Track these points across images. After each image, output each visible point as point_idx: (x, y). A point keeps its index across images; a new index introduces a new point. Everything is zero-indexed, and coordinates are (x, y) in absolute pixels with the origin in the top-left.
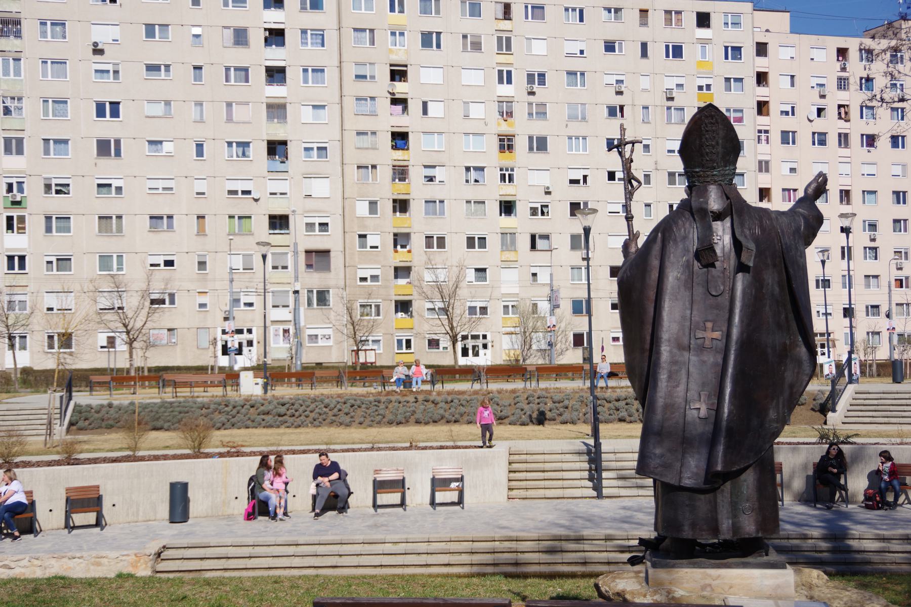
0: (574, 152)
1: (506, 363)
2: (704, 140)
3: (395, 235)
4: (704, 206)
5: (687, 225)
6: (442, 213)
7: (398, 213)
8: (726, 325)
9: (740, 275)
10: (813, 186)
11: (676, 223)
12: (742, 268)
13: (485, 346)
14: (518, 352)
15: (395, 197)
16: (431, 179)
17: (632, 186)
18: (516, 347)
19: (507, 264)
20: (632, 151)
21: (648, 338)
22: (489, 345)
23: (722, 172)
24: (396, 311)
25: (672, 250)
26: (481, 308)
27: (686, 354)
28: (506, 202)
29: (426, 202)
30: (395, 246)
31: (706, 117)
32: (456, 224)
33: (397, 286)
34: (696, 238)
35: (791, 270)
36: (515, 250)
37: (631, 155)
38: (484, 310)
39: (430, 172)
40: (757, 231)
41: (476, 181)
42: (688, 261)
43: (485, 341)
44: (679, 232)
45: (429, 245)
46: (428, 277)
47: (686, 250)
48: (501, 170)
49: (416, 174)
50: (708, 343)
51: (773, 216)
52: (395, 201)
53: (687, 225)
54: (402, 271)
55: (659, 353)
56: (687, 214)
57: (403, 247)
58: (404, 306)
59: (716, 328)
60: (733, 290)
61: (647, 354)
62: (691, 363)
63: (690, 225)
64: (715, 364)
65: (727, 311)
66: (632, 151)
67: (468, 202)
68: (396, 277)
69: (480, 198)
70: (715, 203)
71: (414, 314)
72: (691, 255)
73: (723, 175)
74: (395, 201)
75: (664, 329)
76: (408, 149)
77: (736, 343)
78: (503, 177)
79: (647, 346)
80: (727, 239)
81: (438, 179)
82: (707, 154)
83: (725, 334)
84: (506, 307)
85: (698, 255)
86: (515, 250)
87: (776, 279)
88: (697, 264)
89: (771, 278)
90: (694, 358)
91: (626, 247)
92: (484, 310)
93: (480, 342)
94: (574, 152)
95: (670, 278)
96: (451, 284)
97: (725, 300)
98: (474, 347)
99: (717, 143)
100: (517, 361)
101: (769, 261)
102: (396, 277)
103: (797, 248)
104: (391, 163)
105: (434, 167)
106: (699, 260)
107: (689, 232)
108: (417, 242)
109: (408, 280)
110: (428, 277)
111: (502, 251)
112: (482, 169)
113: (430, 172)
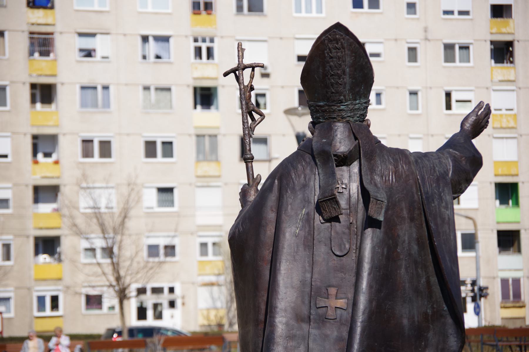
0: (303, 14)
1: (204, 330)
2: (328, 68)
3: (35, 137)
4: (327, 148)
5: (308, 171)
6: (107, 104)
7: (38, 105)
8: (352, 290)
9: (369, 231)
10: (473, 118)
11: (295, 168)
12: (371, 222)
13: (172, 304)
14: (222, 312)
15: (35, 80)
16: (89, 53)
17: (253, 119)
18: (219, 304)
19: (205, 181)
20: (252, 77)
21: (263, 307)
22: (179, 303)
23: (351, 107)
24: (37, 253)
25: (290, 201)
26: (166, 247)
27: (305, 326)
28: (203, 89)
29: (83, 88)
30: (35, 154)
31: (330, 41)
32: (127, 123)
33: (38, 216)
34: (317, 186)
35: (432, 225)
36: (217, 160)
37: (251, 82)
38: (170, 250)
40: (392, 178)
41: (158, 57)
42: (308, 214)
43: (172, 297)
44: (298, 180)
45: (87, 153)
46: (84, 203)
47: (306, 201)
48: (196, 40)
49: (66, 46)
50: (331, 313)
51: (412, 159)
52: (33, 86)
53: (308, 171)
54: (44, 193)
55: (273, 325)
56: (308, 157)
57: (47, 155)
58: (48, 245)
59: (340, 295)
60: (360, 249)
61: (262, 326)
62: (311, 338)
63: (311, 171)
64: (339, 339)
65: (353, 274)
66: (252, 77)
67: (147, 88)
68: (36, 200)
69: (163, 83)
70: (342, 143)
71: (63, 257)
72: (312, 206)
73: (352, 110)
74: (33, 86)
75: (280, 297)
76: (52, 8)
77: (363, 314)
78: (198, 52)
79: (262, 317)
80: (355, 187)
81: (99, 54)
82: (332, 85)
83: (351, 302)
84: (204, 245)
85: (319, 208)
86: (217, 160)
87: (414, 235)
88: (318, 218)
89: (406, 232)
90: (313, 331)
91: (244, 194)
92: (170, 250)
93: (164, 298)
94: (303, 14)
95: (288, 235)
96: (116, 211)
97: (350, 261)
98: (156, 306)
99: (344, 72)
100: (220, 326)
101: (405, 213)
102: (36, 200)
103: (441, 198)
104: (26, 28)
105: (93, 35)
106: (320, 214)
107: (310, 179)
108: (69, 149)
109: (54, 206)
110: (84, 203)
111: (198, 161)
112: (165, 39)
113: (87, 43)
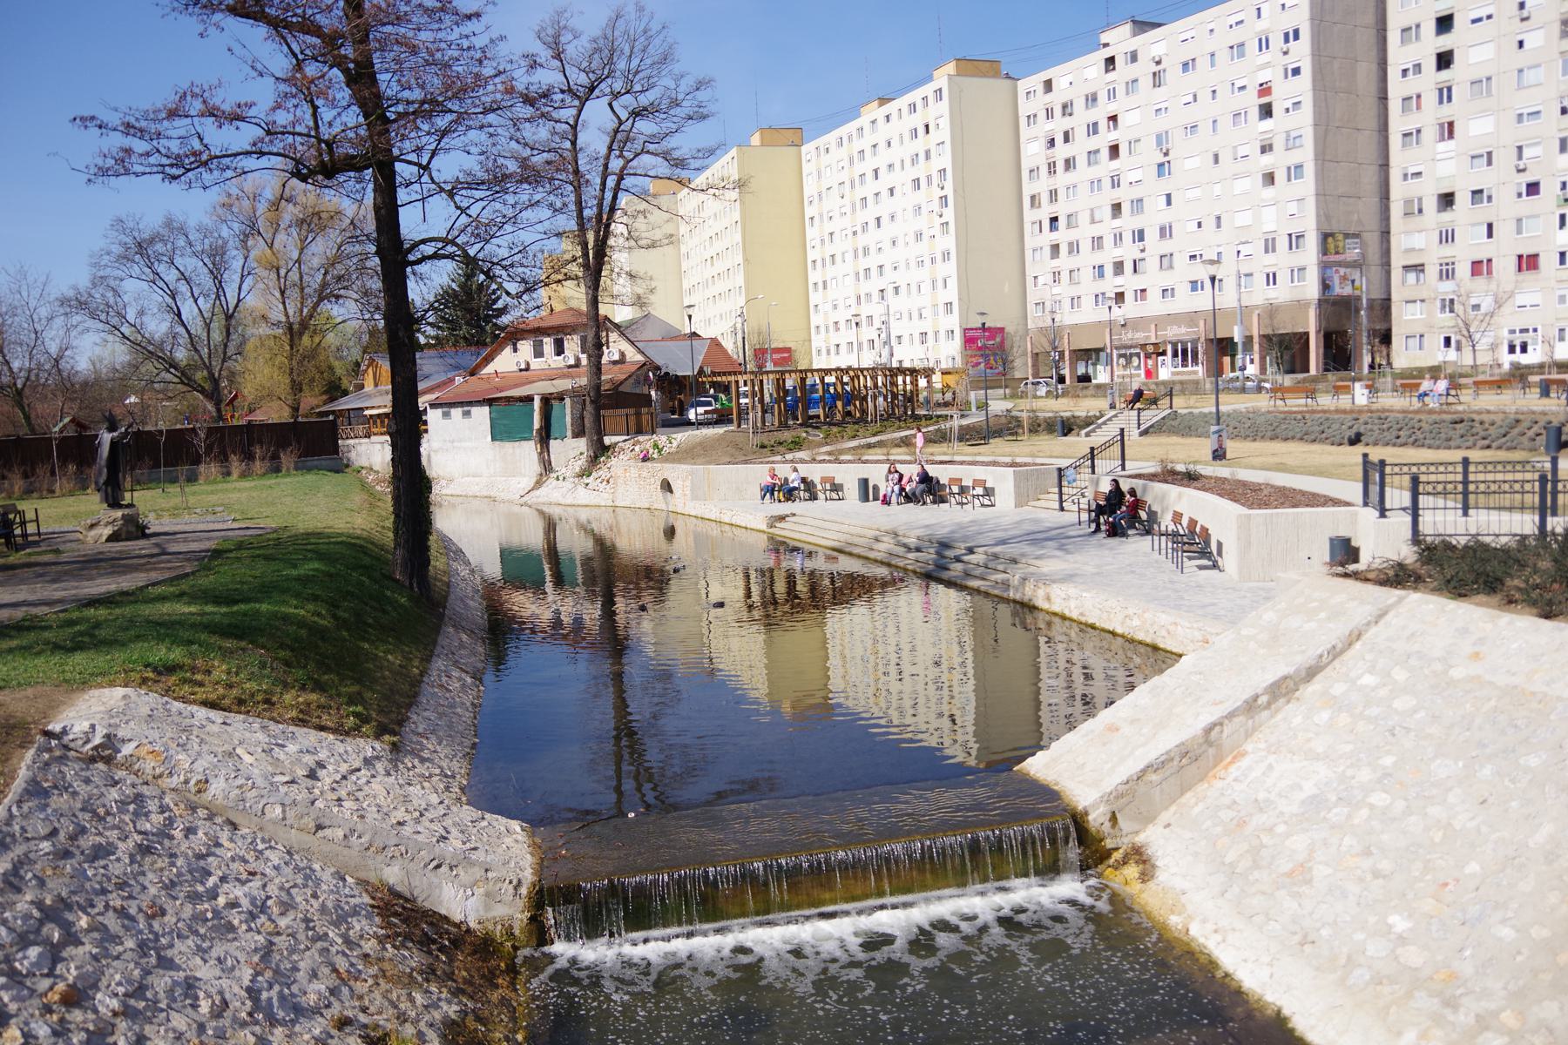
39: (1060, 166)
113: (1060, 166)
